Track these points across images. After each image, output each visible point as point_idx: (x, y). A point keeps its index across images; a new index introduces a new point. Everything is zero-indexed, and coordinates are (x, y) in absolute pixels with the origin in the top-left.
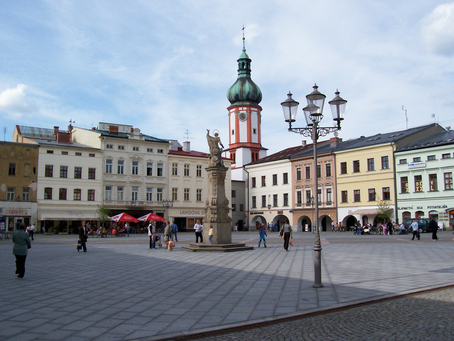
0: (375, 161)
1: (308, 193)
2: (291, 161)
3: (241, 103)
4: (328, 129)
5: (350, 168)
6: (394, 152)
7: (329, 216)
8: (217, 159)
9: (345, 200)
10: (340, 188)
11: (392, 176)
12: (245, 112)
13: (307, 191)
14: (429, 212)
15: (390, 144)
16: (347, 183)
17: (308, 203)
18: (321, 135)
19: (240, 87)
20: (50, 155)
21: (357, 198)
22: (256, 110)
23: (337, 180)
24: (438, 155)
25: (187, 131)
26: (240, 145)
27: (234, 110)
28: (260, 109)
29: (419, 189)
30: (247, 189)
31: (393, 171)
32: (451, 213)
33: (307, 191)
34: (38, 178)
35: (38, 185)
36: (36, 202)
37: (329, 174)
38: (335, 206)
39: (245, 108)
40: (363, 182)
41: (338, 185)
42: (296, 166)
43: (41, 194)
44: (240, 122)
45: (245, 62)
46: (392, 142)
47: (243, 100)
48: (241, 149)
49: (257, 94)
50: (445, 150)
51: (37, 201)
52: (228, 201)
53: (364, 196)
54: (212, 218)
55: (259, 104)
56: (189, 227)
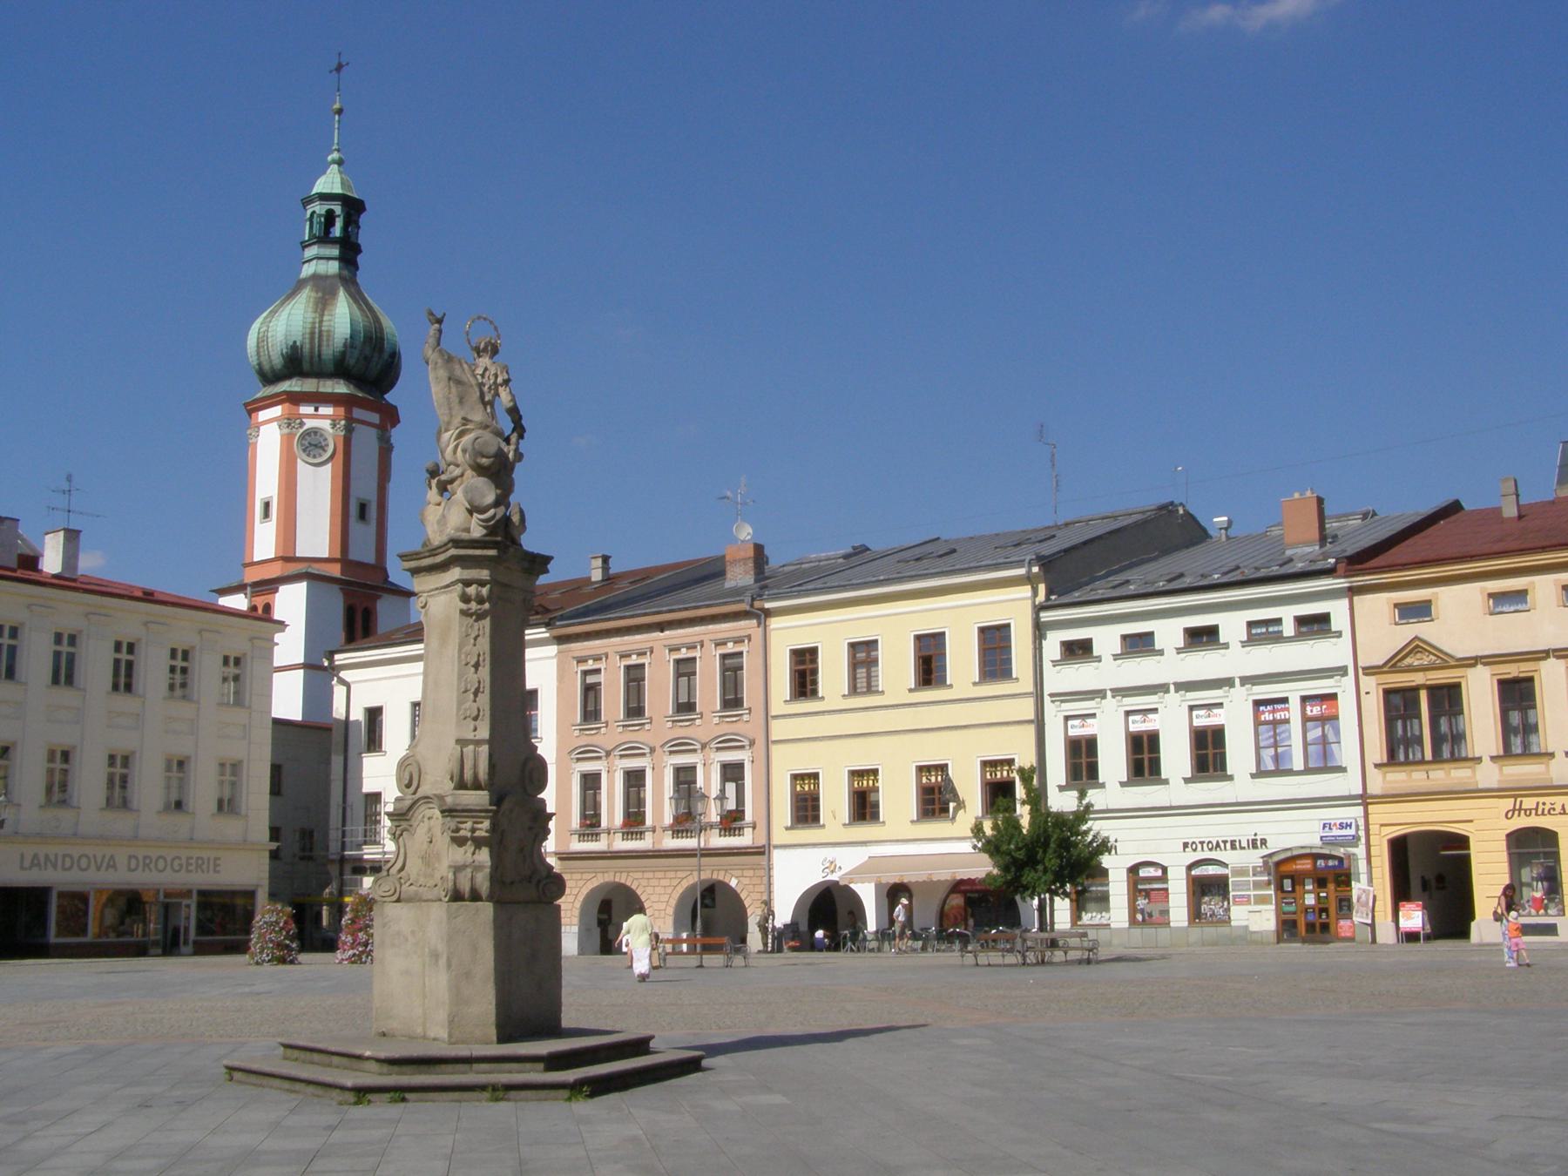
0: (882, 653)
1: (685, 776)
2: (561, 640)
3: (309, 385)
5: (833, 673)
6: (1038, 609)
7: (733, 883)
8: (490, 498)
9: (807, 810)
10: (786, 763)
11: (1026, 709)
12: (326, 424)
13: (679, 771)
14: (1190, 867)
15: (1022, 571)
16: (815, 742)
17: (685, 821)
19: (310, 316)
21: (864, 807)
22: (375, 418)
23: (774, 724)
24: (1232, 626)
25: (69, 478)
26: (292, 567)
27: (277, 411)
28: (390, 416)
29: (1326, 754)
30: (337, 761)
31: (1031, 688)
32: (1284, 868)
33: (679, 771)
37: (732, 700)
38: (762, 841)
39: (327, 410)
40: (896, 736)
41: (774, 749)
42: (581, 660)
44: (303, 469)
45: (338, 209)
46: (1030, 565)
47: (319, 374)
48: (301, 588)
49: (381, 349)
50: (1198, 611)
52: (542, 764)
53: (898, 797)
54: (457, 869)
55: (390, 397)
56: (59, 934)
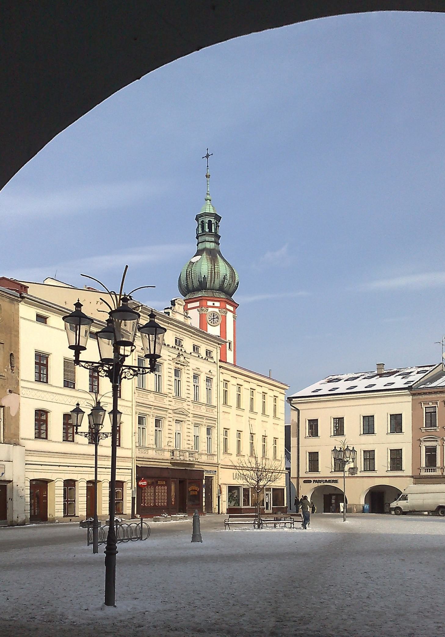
2: (413, 395)
3: (210, 294)
4: (136, 369)
13: (428, 449)
18: (125, 377)
20: (40, 326)
34: (22, 384)
35: (22, 400)
36: (17, 444)
39: (217, 304)
43: (27, 426)
51: (21, 441)
